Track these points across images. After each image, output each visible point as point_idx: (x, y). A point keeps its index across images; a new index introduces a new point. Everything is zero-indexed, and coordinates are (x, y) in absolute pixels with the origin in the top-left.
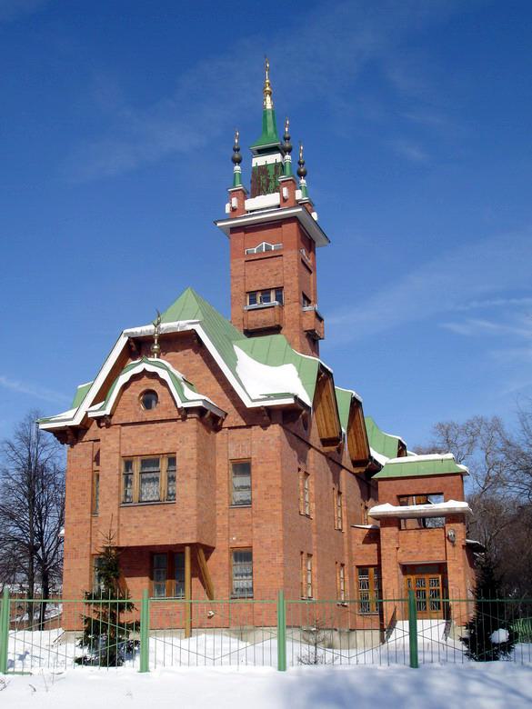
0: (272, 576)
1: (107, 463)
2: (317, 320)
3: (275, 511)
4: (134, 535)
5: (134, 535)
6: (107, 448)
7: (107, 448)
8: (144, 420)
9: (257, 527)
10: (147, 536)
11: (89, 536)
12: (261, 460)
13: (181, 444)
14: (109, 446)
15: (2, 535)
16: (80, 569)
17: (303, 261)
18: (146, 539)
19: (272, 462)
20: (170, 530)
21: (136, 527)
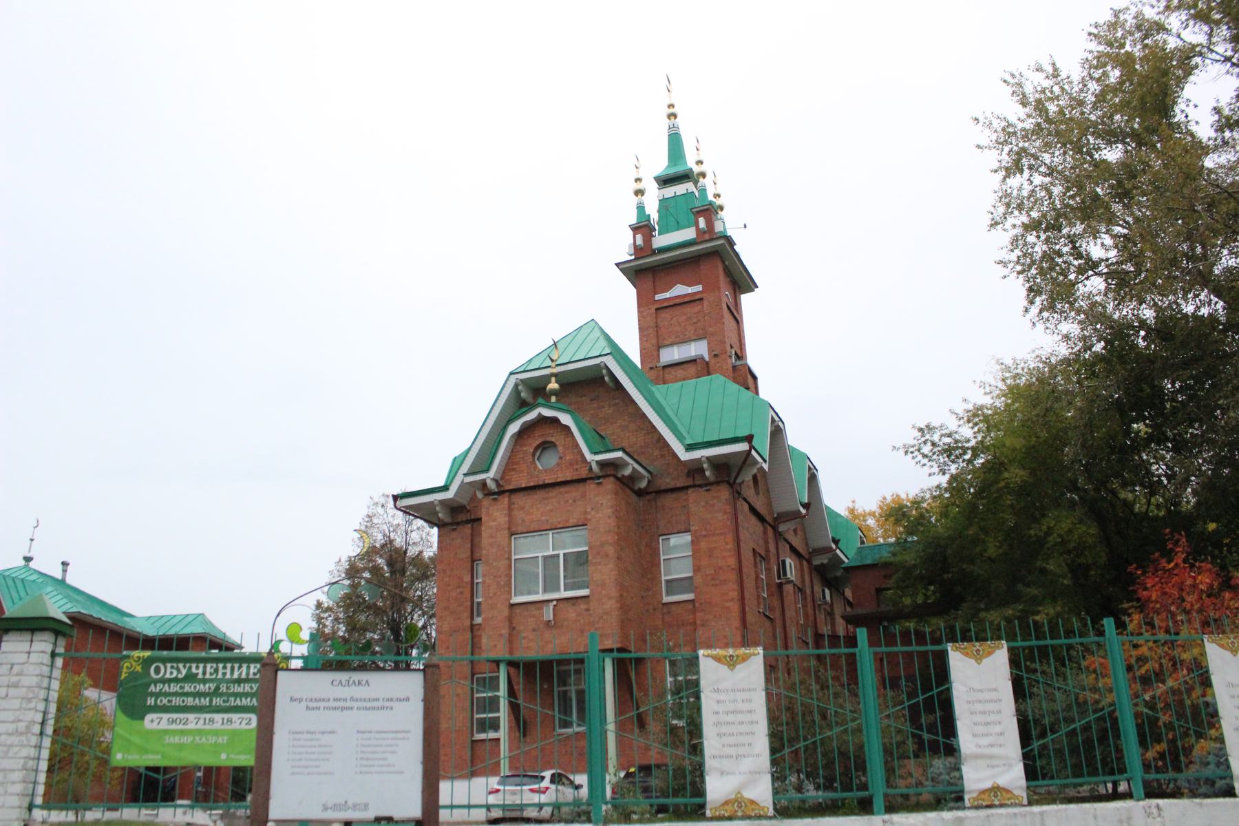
18: (550, 646)
21: (534, 630)
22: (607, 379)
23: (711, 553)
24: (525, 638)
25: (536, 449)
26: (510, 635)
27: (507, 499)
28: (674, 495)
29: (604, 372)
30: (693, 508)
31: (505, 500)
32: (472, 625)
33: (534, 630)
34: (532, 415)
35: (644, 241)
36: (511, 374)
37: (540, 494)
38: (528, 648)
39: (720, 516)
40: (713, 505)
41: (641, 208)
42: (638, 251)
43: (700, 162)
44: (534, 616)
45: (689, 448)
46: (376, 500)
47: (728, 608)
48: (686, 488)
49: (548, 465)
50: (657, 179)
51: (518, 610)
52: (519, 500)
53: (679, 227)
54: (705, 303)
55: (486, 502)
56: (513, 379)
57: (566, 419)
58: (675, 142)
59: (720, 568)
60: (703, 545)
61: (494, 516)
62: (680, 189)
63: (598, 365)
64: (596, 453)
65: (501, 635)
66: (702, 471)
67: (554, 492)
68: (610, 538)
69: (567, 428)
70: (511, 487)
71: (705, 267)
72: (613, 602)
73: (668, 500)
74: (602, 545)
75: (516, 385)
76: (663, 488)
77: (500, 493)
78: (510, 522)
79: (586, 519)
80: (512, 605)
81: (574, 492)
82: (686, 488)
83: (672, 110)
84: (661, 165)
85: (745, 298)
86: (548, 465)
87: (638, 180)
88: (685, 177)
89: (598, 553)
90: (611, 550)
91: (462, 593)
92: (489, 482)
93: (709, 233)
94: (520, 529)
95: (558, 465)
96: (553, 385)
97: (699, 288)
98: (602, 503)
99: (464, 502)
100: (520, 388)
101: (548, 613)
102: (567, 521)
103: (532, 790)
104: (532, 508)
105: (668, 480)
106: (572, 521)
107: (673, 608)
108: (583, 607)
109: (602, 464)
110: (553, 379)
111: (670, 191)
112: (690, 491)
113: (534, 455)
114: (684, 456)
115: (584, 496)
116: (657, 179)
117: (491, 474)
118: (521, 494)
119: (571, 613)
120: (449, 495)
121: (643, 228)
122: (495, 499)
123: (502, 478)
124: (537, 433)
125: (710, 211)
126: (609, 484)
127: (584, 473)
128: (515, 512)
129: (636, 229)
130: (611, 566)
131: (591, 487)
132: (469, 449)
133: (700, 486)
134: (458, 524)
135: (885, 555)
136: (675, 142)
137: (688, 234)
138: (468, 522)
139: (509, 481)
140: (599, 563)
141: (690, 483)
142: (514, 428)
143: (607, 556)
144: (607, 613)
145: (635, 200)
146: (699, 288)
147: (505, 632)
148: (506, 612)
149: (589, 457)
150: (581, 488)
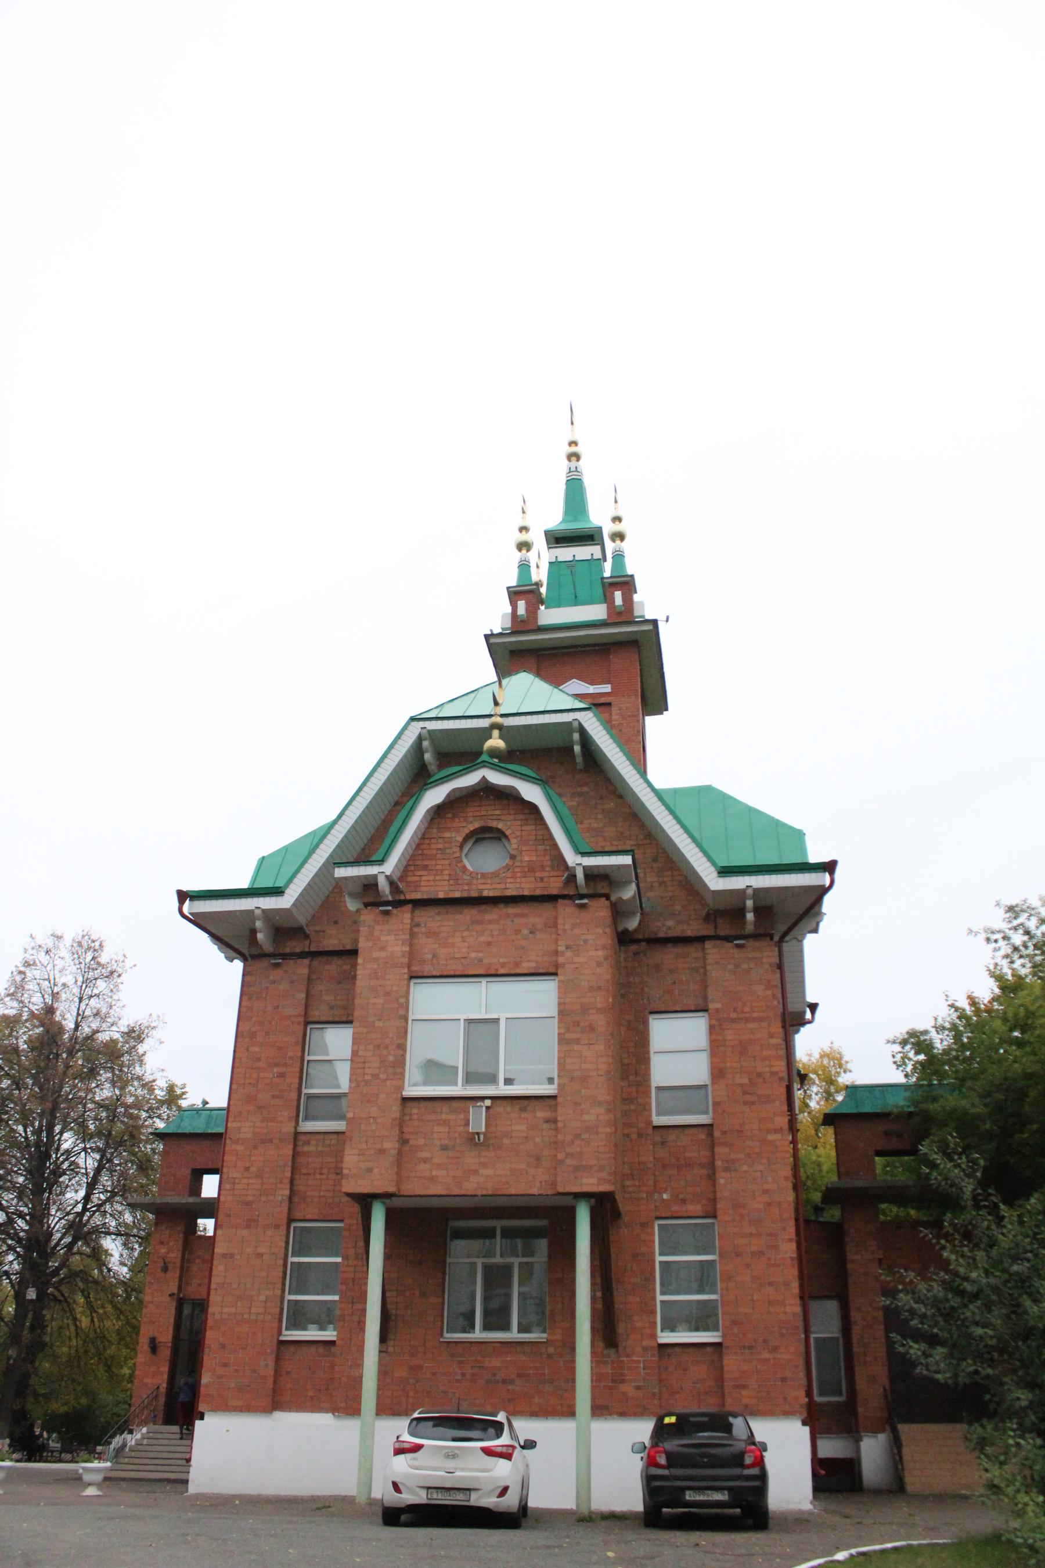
0: (771, 1290)
1: (373, 989)
2: (499, 1490)
3: (769, 1131)
4: (440, 1166)
5: (440, 1166)
6: (377, 954)
7: (377, 954)
8: (474, 894)
9: (726, 1170)
10: (475, 1172)
11: (289, 1174)
12: (734, 1015)
13: (568, 954)
14: (383, 949)
15: (6, 1083)
16: (259, 1256)
17: (392, 1516)
18: (474, 1179)
19: (761, 1019)
20: (538, 1159)
21: (444, 1148)
22: (577, 749)
23: (743, 1049)
24: (425, 1161)
25: (466, 839)
26: (400, 1153)
27: (408, 916)
28: (679, 949)
29: (576, 736)
30: (714, 973)
31: (405, 916)
32: (297, 1134)
33: (444, 1148)
34: (470, 780)
35: (527, 610)
36: (413, 719)
37: (469, 914)
38: (432, 1179)
39: (760, 990)
40: (748, 972)
41: (524, 567)
42: (520, 625)
43: (617, 519)
44: (444, 1123)
45: (725, 871)
46: (39, 941)
47: (772, 1142)
48: (701, 939)
49: (485, 864)
50: (547, 533)
51: (414, 1110)
52: (431, 919)
53: (576, 601)
54: (615, 710)
55: (368, 917)
56: (416, 729)
57: (531, 792)
58: (575, 493)
59: (759, 1075)
60: (729, 1035)
61: (383, 941)
62: (583, 552)
63: (569, 724)
64: (583, 854)
65: (382, 1151)
66: (741, 911)
67: (493, 914)
68: (600, 1000)
69: (532, 809)
70: (418, 896)
71: (618, 661)
72: (601, 1110)
73: (667, 956)
74: (585, 1009)
75: (420, 739)
76: (661, 934)
77: (398, 904)
78: (412, 954)
79: (557, 966)
80: (406, 1100)
81: (536, 916)
82: (701, 939)
83: (573, 449)
84: (554, 518)
85: (651, 721)
86: (485, 864)
87: (523, 529)
88: (590, 537)
89: (577, 1024)
90: (600, 1021)
91: (282, 1075)
92: (382, 882)
93: (625, 614)
94: (427, 969)
95: (507, 867)
96: (496, 742)
97: (607, 688)
98: (587, 939)
99: (302, 921)
100: (426, 744)
101: (478, 1120)
102: (517, 964)
103: (488, 1452)
104: (457, 935)
105: (670, 923)
106: (526, 966)
107: (672, 1136)
108: (541, 1114)
109: (592, 875)
110: (496, 733)
111: (566, 553)
112: (708, 944)
113: (461, 847)
114: (715, 883)
115: (552, 925)
116: (547, 533)
117: (389, 867)
118: (432, 911)
119: (517, 1125)
120: (285, 902)
121: (524, 593)
122: (387, 913)
123: (402, 878)
124: (471, 812)
125: (626, 584)
126: (600, 910)
127: (555, 885)
128: (422, 940)
129: (514, 595)
130: (601, 1047)
131: (566, 911)
132: (335, 823)
133: (727, 939)
134: (285, 956)
135: (899, 1102)
136: (575, 493)
137: (597, 612)
138: (302, 955)
139: (417, 887)
140: (577, 1041)
141: (708, 930)
142: (435, 796)
143: (592, 1029)
144: (588, 1129)
145: (517, 556)
146: (607, 688)
147: (391, 1145)
148: (395, 1111)
149: (571, 858)
150: (546, 911)
